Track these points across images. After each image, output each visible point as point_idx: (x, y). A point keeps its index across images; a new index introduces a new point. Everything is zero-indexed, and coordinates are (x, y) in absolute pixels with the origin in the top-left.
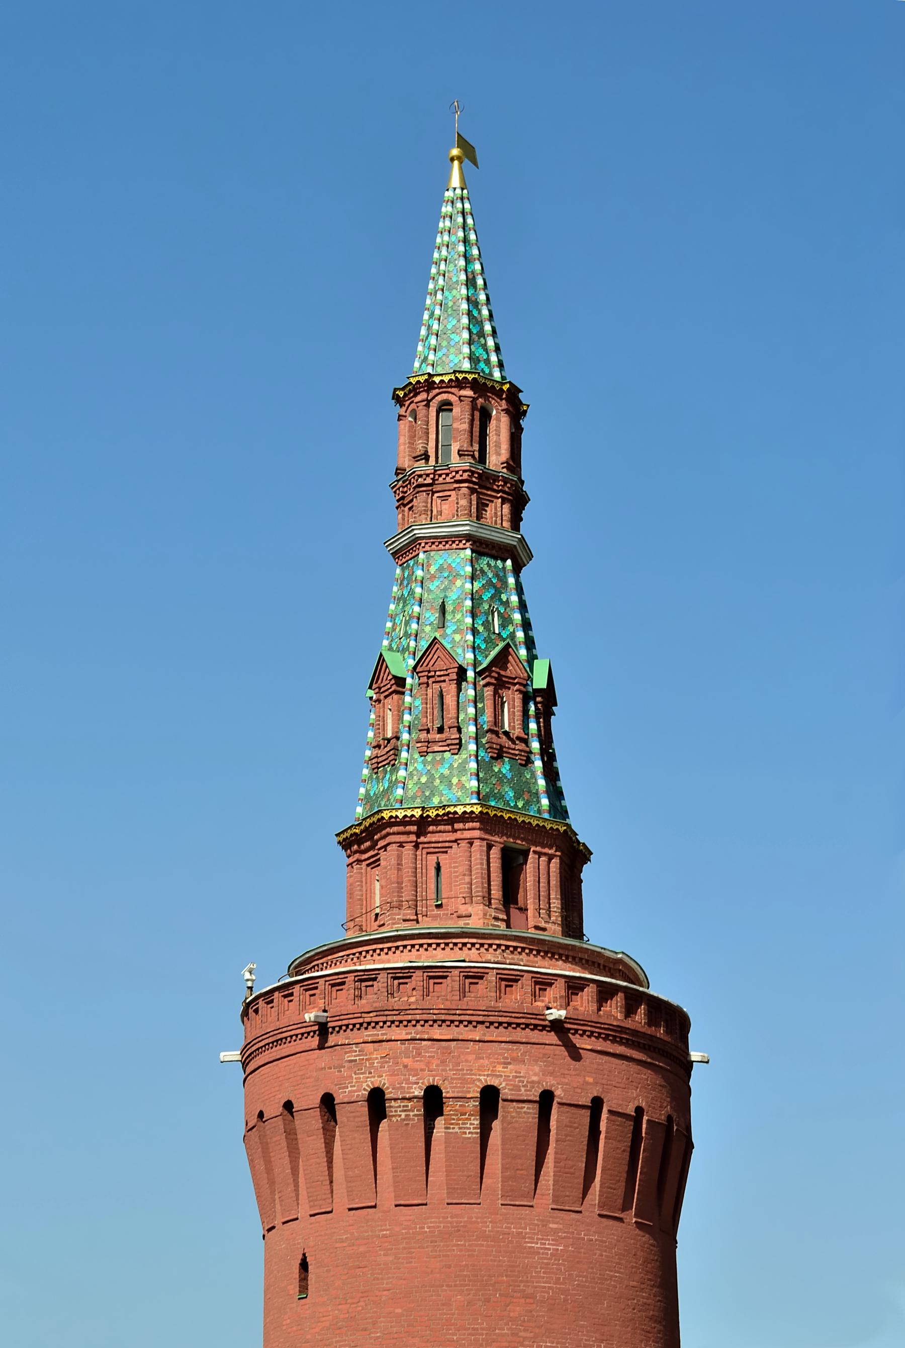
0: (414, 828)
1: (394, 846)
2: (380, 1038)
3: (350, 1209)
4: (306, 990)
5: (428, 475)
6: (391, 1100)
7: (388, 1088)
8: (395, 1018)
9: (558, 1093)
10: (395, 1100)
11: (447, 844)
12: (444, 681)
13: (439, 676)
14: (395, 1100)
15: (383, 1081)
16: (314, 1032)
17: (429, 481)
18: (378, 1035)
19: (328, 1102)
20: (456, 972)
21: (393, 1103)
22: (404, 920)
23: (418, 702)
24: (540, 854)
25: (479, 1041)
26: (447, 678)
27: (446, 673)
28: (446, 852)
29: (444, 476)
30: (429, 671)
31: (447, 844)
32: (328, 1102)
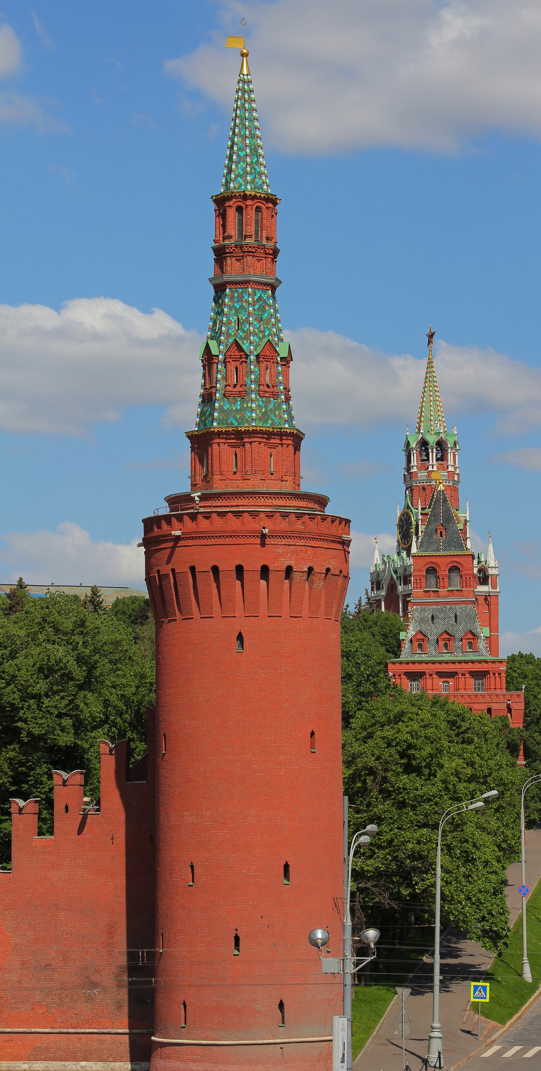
0: (266, 436)
1: (257, 443)
2: (290, 543)
3: (269, 616)
4: (250, 516)
5: (254, 247)
6: (295, 572)
7: (294, 566)
8: (298, 535)
9: (332, 570)
10: (297, 572)
11: (277, 445)
12: (270, 361)
13: (268, 359)
14: (297, 572)
15: (292, 563)
16: (258, 536)
17: (254, 250)
18: (289, 542)
19: (240, 569)
20: (319, 517)
21: (323, 572)
22: (261, 480)
23: (256, 370)
24: (251, 443)
25: (326, 548)
26: (272, 361)
27: (271, 357)
28: (275, 448)
29: (260, 249)
30: (264, 356)
31: (277, 445)
32: (215, 569)
